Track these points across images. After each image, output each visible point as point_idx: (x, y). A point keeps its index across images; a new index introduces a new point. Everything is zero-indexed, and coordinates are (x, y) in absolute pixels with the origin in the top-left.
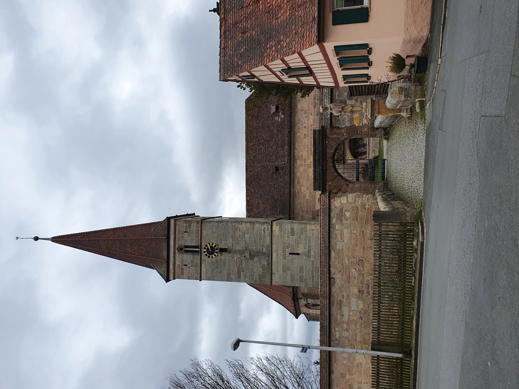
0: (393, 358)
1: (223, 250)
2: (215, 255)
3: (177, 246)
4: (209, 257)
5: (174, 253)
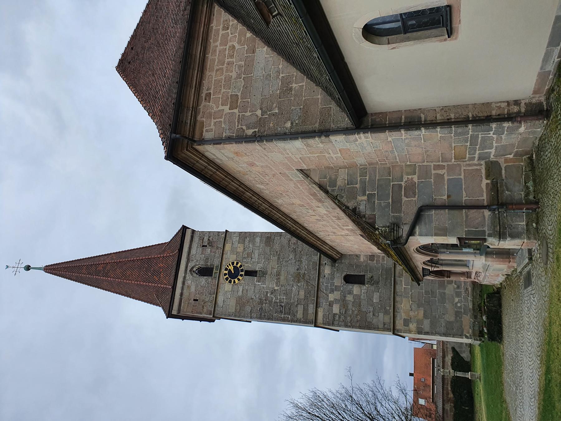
0: (488, 406)
2: (239, 280)
4: (230, 282)
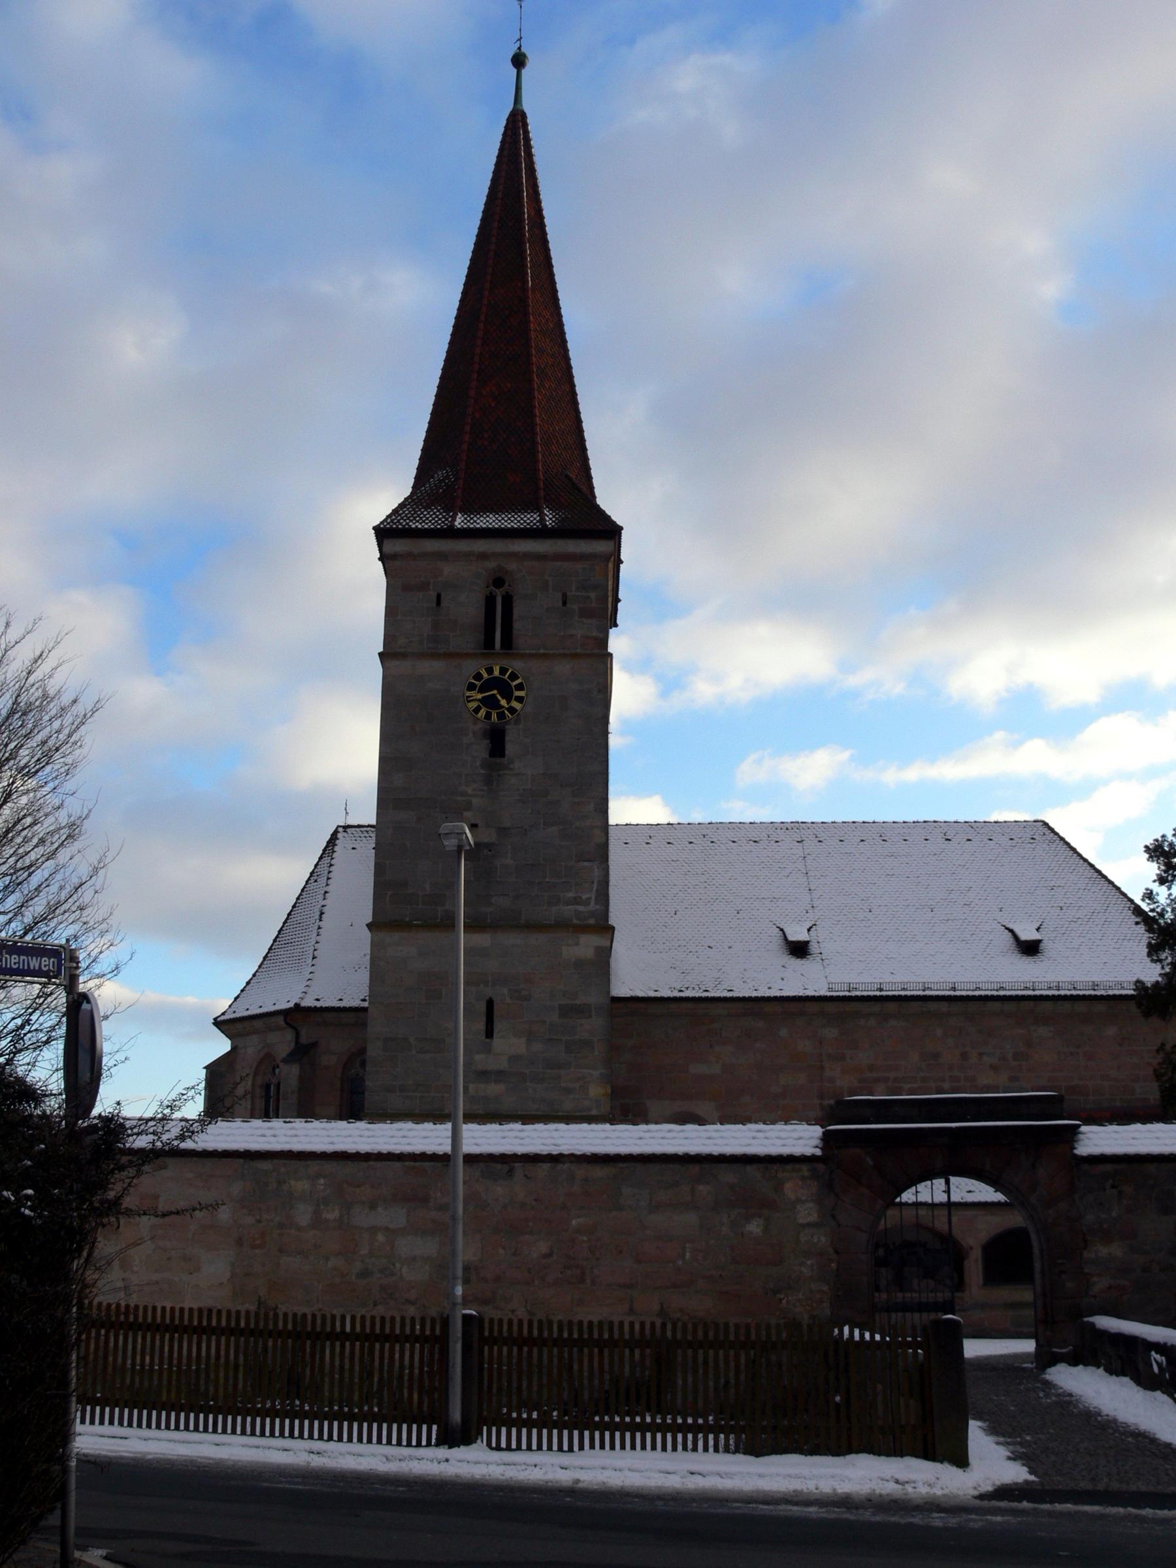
1: (496, 740)
3: (512, 566)
5: (483, 556)
